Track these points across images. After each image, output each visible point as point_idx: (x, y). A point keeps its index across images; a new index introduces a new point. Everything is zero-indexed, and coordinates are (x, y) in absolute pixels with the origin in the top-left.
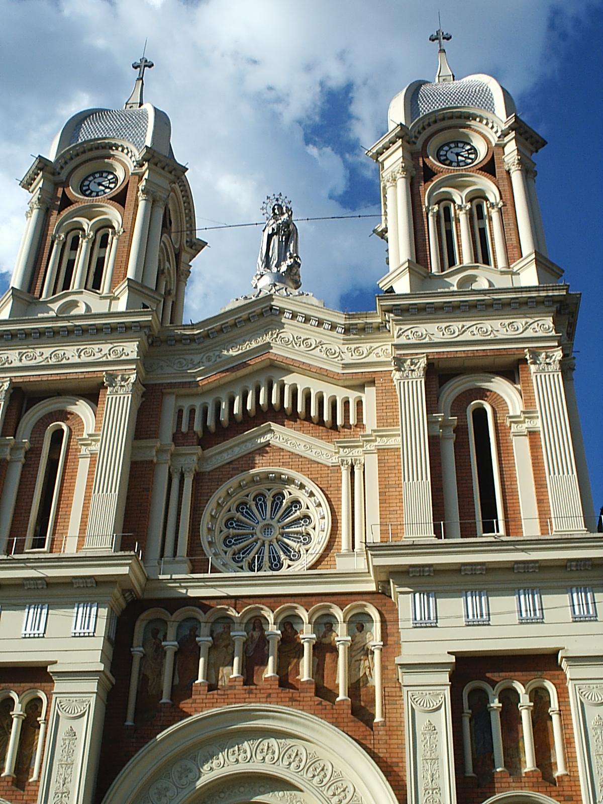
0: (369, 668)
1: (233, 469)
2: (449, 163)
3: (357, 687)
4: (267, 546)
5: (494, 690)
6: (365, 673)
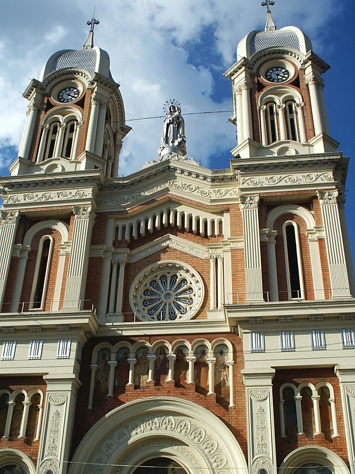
0: (226, 376)
1: (148, 261)
2: (273, 80)
3: (219, 387)
4: (167, 305)
5: (297, 388)
6: (224, 379)
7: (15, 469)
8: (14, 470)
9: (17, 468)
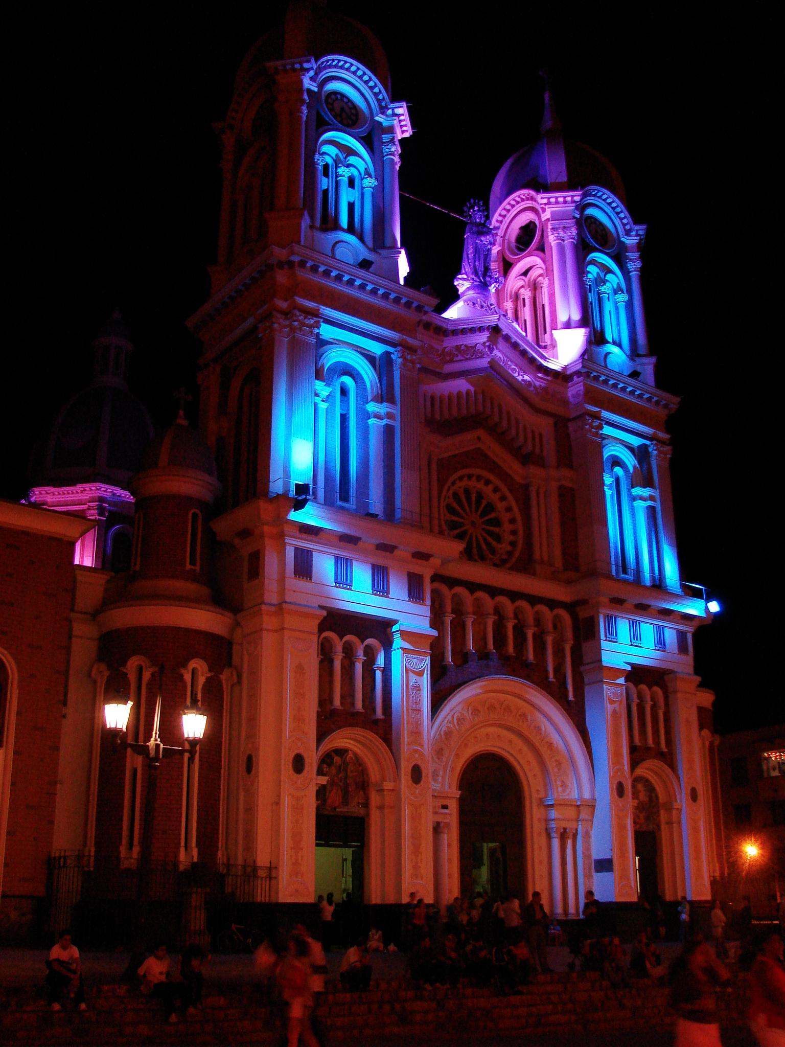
7: (347, 755)
8: (346, 757)
9: (350, 755)
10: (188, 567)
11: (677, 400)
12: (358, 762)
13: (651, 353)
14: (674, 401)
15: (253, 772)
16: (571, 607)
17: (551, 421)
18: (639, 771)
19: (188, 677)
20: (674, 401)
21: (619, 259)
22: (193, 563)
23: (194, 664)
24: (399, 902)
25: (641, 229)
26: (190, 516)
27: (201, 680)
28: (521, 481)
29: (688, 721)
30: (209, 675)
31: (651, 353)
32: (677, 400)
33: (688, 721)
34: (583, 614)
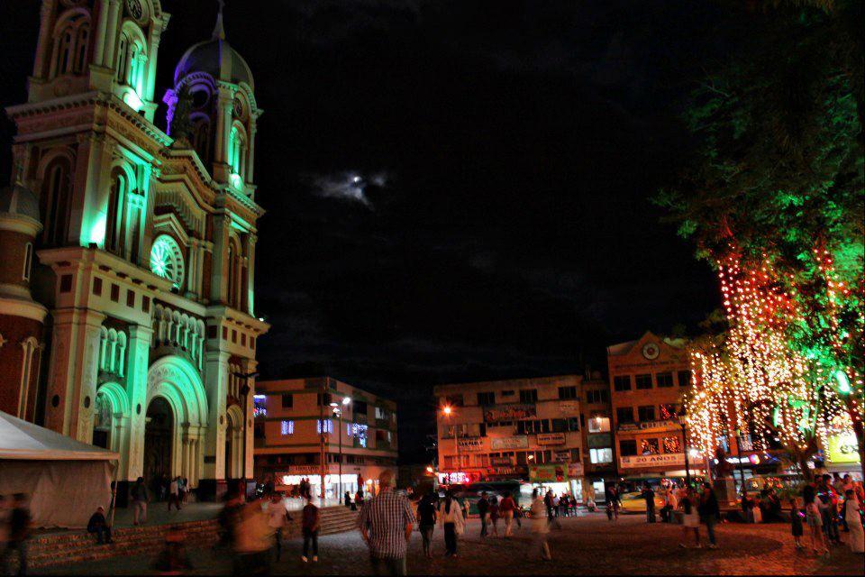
9: (104, 396)
10: (24, 278)
11: (265, 211)
12: (108, 402)
13: (254, 183)
14: (263, 211)
15: (60, 406)
16: (204, 319)
17: (205, 213)
18: (230, 411)
19: (25, 347)
20: (263, 211)
21: (146, 30)
22: (26, 276)
23: (31, 340)
24: (211, 478)
25: (167, 17)
26: (27, 248)
27: (32, 350)
28: (186, 245)
29: (141, 358)
30: (4, 341)
31: (254, 183)
32: (265, 211)
33: (141, 358)
34: (211, 323)
